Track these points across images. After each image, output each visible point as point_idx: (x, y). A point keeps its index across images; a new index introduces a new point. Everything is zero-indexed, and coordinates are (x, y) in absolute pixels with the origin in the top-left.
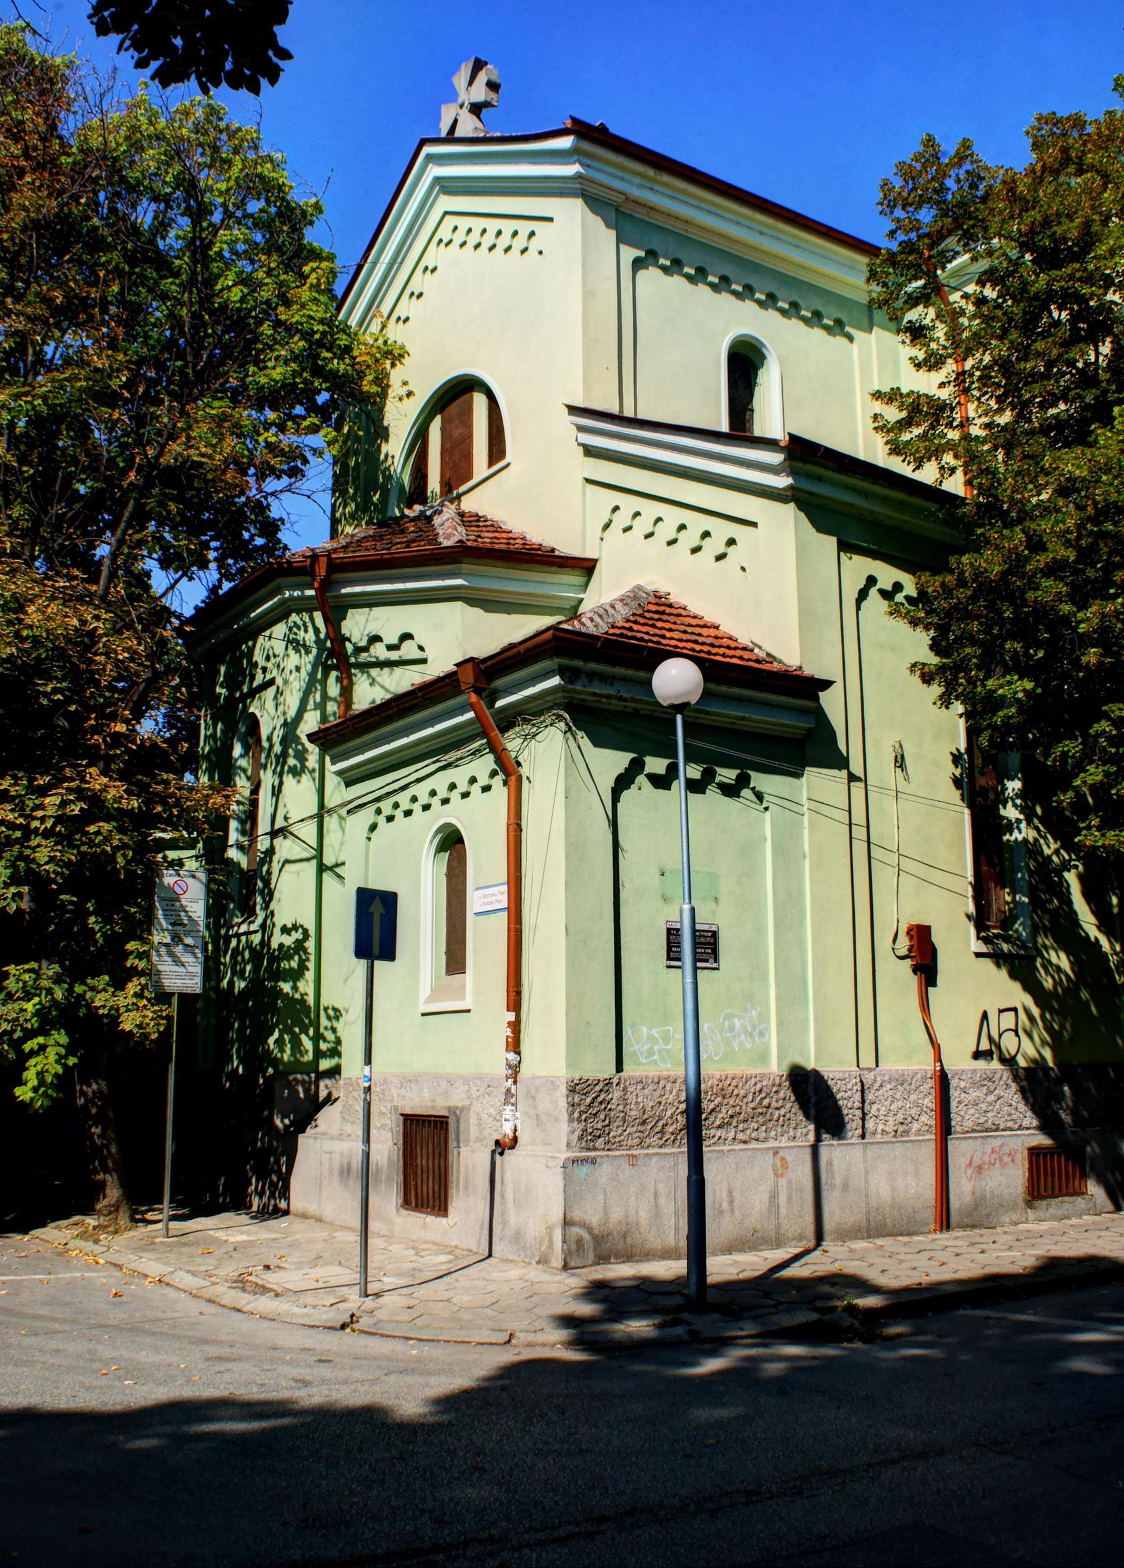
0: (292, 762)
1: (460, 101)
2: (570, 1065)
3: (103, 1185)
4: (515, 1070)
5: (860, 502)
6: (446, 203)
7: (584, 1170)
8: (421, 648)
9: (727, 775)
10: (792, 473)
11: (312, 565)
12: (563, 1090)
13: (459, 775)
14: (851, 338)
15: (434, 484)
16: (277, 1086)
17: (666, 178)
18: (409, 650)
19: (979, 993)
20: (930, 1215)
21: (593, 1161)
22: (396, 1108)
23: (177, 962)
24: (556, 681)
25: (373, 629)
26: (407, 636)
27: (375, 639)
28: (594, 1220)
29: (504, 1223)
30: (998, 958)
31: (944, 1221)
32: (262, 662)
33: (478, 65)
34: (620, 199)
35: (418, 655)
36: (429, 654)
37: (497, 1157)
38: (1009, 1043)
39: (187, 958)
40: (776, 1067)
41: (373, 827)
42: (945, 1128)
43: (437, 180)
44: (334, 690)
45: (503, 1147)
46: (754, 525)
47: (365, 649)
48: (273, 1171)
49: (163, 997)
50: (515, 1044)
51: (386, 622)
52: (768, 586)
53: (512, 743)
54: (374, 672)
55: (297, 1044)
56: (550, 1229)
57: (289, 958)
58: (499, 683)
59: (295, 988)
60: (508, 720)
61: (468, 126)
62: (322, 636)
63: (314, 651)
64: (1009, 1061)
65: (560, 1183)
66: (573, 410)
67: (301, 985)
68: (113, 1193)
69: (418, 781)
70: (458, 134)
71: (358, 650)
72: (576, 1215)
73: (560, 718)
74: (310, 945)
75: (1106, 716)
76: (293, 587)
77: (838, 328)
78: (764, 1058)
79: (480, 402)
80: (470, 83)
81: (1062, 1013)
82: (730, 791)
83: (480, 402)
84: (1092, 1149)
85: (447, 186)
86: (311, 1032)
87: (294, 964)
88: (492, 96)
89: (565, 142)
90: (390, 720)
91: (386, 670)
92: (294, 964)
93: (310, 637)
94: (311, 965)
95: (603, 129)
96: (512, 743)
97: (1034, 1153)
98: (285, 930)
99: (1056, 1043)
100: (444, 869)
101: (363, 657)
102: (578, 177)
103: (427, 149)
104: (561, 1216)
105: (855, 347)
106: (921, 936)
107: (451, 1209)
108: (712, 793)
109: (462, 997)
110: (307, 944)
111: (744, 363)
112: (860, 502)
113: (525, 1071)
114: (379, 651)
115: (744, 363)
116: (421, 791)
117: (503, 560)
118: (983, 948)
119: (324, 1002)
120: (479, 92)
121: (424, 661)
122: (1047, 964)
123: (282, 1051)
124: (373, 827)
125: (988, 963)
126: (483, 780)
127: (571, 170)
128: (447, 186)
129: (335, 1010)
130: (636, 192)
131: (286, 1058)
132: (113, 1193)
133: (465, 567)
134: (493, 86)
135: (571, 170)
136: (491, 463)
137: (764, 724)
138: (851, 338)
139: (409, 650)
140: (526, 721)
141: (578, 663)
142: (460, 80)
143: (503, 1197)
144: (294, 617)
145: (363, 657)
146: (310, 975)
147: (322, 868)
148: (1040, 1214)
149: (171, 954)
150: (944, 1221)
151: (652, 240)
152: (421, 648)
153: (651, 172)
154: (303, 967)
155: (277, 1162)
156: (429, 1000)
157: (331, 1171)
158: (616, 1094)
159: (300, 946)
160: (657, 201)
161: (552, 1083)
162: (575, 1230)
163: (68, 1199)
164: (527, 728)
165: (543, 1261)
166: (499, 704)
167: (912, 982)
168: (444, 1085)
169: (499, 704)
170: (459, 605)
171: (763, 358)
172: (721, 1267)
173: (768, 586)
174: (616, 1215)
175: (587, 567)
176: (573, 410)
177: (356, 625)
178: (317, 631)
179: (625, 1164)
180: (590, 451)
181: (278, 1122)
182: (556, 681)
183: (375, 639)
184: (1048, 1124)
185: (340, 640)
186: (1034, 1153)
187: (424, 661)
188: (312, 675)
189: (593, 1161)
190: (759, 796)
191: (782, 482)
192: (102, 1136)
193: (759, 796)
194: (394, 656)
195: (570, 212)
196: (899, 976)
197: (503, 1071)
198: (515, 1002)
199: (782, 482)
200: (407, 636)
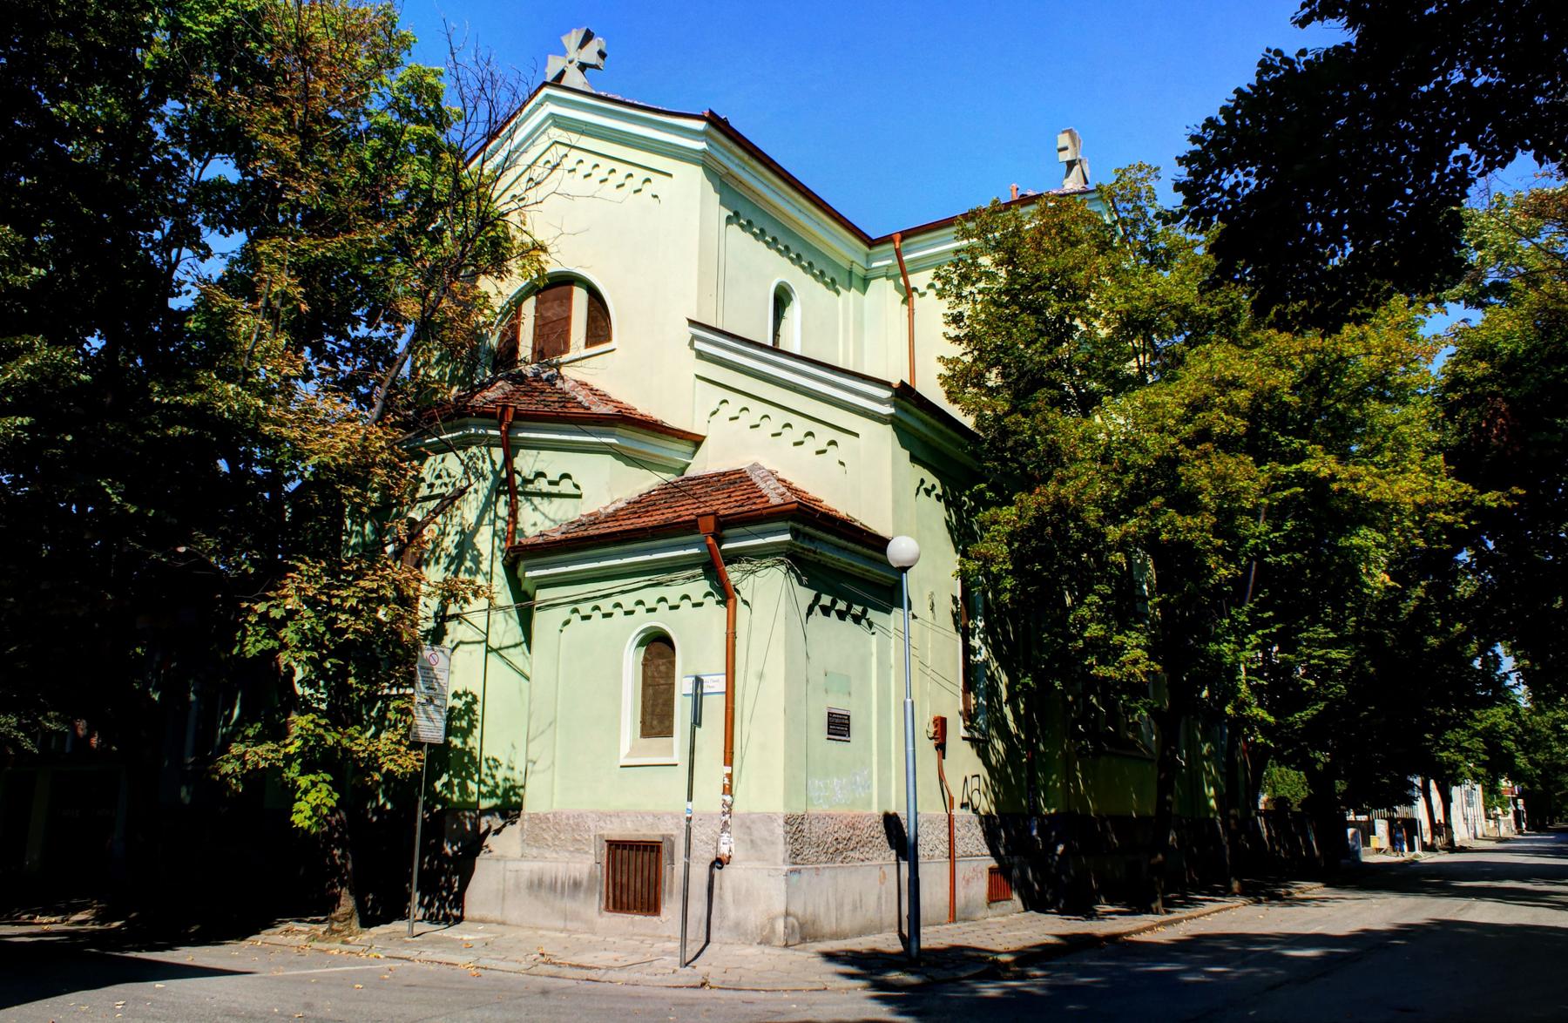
0: (468, 564)
1: (570, 57)
2: (786, 804)
3: (337, 898)
4: (728, 809)
5: (923, 429)
6: (556, 134)
7: (795, 877)
8: (577, 487)
9: (857, 609)
10: (895, 405)
11: (502, 413)
12: (781, 822)
13: (673, 593)
14: (838, 293)
15: (525, 349)
16: (447, 818)
17: (754, 163)
18: (566, 487)
19: (964, 763)
20: (946, 912)
21: (799, 872)
22: (601, 836)
23: (430, 719)
24: (787, 537)
25: (539, 467)
26: (566, 476)
27: (540, 475)
28: (800, 913)
29: (723, 917)
30: (972, 740)
31: (953, 918)
32: (429, 479)
33: (588, 37)
34: (723, 171)
35: (576, 492)
36: (583, 491)
37: (716, 871)
38: (976, 798)
39: (436, 716)
40: (876, 811)
41: (567, 623)
42: (952, 856)
43: (552, 115)
44: (503, 510)
45: (719, 863)
46: (857, 435)
47: (531, 482)
48: (443, 888)
49: (416, 745)
50: (728, 790)
51: (553, 463)
52: (872, 481)
53: (733, 574)
54: (537, 500)
55: (464, 789)
56: (772, 920)
57: (461, 718)
58: (727, 532)
59: (465, 743)
60: (734, 558)
61: (574, 78)
62: (498, 467)
63: (491, 477)
64: (975, 810)
65: (783, 886)
66: (692, 323)
67: (470, 741)
68: (347, 903)
69: (623, 592)
70: (564, 82)
71: (526, 481)
72: (792, 909)
73: (782, 562)
74: (478, 708)
75: (1094, 592)
76: (477, 426)
77: (832, 285)
78: (869, 804)
79: (580, 297)
80: (582, 46)
81: (999, 781)
82: (857, 620)
83: (580, 297)
84: (1016, 873)
85: (557, 121)
86: (476, 777)
87: (464, 724)
88: (599, 62)
89: (700, 125)
90: (606, 545)
91: (546, 500)
92: (464, 724)
93: (487, 467)
94: (479, 725)
95: (725, 122)
96: (733, 574)
97: (991, 870)
98: (456, 695)
99: (997, 803)
100: (641, 659)
101: (530, 488)
102: (704, 151)
103: (546, 91)
104: (783, 909)
105: (840, 299)
106: (941, 723)
107: (663, 910)
108: (849, 619)
109: (671, 754)
110: (475, 707)
111: (782, 299)
112: (923, 429)
113: (735, 809)
114: (542, 485)
115: (782, 299)
116: (628, 601)
117: (628, 429)
118: (967, 735)
119: (486, 754)
120: (590, 54)
121: (579, 496)
122: (994, 747)
123: (452, 792)
124: (567, 623)
125: (967, 743)
126: (697, 598)
127: (700, 145)
128: (557, 121)
129: (495, 760)
130: (736, 170)
131: (455, 797)
132: (347, 903)
133: (618, 430)
134: (602, 54)
135: (700, 145)
136: (589, 344)
137: (844, 567)
138: (838, 293)
139: (566, 487)
140: (749, 562)
141: (800, 527)
142: (572, 40)
143: (721, 897)
144: (474, 449)
145: (530, 488)
146: (477, 732)
147: (489, 650)
148: (999, 911)
149: (425, 712)
150: (953, 918)
151: (742, 210)
152: (577, 487)
153: (746, 157)
154: (471, 725)
155: (449, 880)
156: (628, 756)
157: (517, 886)
158: (806, 826)
159: (469, 708)
160: (753, 178)
161: (769, 818)
162: (791, 920)
163: (311, 904)
164: (749, 567)
165: (766, 941)
166: (725, 547)
167: (934, 754)
168: (650, 819)
169: (725, 547)
170: (609, 457)
171: (791, 299)
172: (932, 937)
173: (872, 481)
174: (810, 910)
175: (697, 441)
176: (692, 323)
177: (526, 462)
178: (493, 463)
179: (813, 873)
180: (701, 355)
181: (448, 850)
182: (787, 537)
183: (540, 475)
184: (994, 853)
185: (513, 472)
186: (991, 870)
187: (579, 496)
188: (488, 498)
189: (799, 872)
190: (870, 625)
191: (888, 410)
192: (343, 856)
193: (870, 625)
194: (554, 489)
195: (692, 176)
196: (927, 748)
197: (719, 809)
198: (729, 760)
199: (888, 410)
200: (566, 476)
